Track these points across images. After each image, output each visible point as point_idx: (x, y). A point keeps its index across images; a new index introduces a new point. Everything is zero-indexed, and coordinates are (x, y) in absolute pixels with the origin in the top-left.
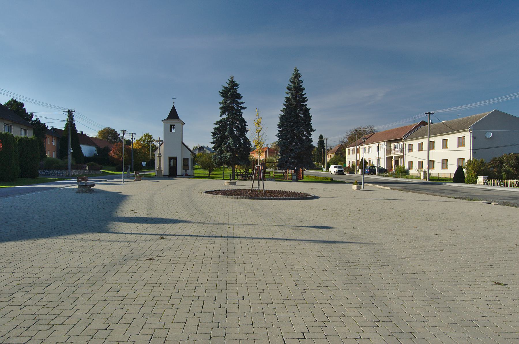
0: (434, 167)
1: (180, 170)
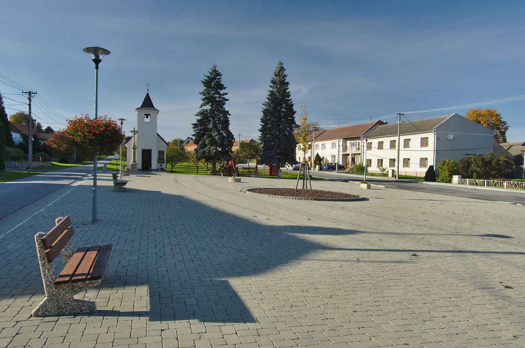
0: (371, 166)
1: (154, 164)
